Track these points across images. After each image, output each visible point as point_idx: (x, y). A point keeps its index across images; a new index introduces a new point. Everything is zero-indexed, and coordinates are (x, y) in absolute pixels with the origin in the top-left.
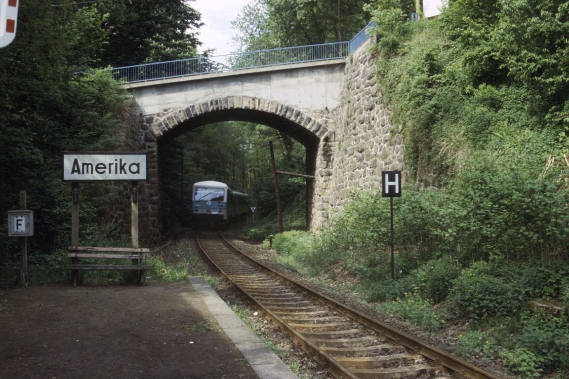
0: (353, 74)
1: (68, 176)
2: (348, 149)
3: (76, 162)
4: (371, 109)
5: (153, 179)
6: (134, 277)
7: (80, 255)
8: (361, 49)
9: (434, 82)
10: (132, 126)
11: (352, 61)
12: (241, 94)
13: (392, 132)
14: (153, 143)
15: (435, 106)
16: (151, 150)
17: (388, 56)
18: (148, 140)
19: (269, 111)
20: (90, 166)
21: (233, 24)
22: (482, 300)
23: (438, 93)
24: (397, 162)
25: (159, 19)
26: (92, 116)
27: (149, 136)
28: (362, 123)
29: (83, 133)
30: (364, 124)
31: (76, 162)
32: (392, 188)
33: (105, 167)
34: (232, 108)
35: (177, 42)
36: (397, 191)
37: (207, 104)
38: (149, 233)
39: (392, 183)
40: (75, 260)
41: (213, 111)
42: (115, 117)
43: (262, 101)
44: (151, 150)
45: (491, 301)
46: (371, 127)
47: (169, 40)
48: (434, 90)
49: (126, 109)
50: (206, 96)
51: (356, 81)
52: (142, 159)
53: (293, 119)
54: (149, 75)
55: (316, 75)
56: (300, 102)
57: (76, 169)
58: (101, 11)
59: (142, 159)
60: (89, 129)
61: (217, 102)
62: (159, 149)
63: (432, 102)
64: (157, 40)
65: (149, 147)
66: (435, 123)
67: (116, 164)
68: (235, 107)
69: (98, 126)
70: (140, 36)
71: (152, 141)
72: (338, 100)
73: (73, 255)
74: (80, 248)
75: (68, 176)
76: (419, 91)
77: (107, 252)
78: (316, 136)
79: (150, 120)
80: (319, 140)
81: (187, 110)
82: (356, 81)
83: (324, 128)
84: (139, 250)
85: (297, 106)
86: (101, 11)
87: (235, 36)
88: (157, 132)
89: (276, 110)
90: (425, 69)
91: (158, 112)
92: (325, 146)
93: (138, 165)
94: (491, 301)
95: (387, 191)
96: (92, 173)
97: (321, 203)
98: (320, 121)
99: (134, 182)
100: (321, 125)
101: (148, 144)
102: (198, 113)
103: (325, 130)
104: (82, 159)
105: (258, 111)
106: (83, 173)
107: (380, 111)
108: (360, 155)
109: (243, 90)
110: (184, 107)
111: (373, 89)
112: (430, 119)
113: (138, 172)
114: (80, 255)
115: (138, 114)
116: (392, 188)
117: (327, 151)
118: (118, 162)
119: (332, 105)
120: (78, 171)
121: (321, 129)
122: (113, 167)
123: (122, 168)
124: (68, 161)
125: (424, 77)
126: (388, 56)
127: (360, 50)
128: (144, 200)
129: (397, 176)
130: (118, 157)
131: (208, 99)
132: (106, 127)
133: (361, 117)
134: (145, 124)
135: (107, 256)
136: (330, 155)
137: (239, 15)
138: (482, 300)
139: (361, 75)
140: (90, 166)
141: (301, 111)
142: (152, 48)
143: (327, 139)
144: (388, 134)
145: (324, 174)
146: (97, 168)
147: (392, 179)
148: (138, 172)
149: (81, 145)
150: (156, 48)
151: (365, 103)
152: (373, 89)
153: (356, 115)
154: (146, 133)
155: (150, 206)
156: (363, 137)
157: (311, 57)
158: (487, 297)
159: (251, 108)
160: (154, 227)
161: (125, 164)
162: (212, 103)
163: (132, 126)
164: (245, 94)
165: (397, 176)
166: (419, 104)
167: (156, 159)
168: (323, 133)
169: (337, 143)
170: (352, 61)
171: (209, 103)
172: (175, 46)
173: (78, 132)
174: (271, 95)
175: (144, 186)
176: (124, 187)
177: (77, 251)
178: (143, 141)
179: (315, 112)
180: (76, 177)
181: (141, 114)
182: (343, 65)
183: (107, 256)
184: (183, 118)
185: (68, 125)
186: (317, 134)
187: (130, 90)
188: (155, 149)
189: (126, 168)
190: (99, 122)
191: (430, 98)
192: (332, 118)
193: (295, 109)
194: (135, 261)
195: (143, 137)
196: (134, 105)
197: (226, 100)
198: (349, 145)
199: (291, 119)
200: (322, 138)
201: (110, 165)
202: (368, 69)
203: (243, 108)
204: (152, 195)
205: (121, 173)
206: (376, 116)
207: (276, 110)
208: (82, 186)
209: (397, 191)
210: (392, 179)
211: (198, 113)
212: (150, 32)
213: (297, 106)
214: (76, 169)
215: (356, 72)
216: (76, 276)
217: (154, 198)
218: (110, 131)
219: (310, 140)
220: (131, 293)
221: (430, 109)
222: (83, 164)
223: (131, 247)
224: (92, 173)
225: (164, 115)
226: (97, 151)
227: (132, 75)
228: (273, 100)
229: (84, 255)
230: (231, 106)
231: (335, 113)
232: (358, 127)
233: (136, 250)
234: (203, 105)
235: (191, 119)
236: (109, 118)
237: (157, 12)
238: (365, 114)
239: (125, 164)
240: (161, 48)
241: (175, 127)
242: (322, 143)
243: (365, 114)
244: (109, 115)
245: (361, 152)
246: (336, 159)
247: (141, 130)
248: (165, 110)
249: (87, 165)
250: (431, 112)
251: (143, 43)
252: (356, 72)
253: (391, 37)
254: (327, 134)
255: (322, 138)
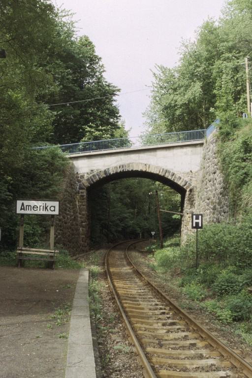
0: (207, 151)
1: (19, 211)
2: (202, 197)
3: (23, 204)
4: (215, 173)
5: (84, 212)
6: (50, 265)
7: (23, 252)
8: (212, 133)
9: (247, 159)
10: (71, 180)
11: (206, 142)
12: (137, 162)
13: (224, 188)
14: (84, 190)
15: (245, 173)
16: (83, 194)
17: (223, 141)
18: (81, 188)
19: (155, 173)
20: (30, 207)
21: (143, 114)
22: (223, 285)
23: (248, 165)
24: (226, 207)
25: (91, 114)
26: (46, 174)
27: (81, 186)
28: (210, 182)
29: (40, 185)
30: (211, 182)
31: (23, 204)
32: (197, 224)
33: (37, 208)
34: (132, 171)
35: (103, 128)
36: (200, 225)
37: (117, 167)
38: (79, 245)
39: (197, 221)
40: (21, 254)
41: (120, 172)
42: (60, 175)
43: (151, 166)
44: (83, 194)
45: (228, 286)
46: (214, 185)
47: (97, 126)
48: (246, 163)
49: (68, 170)
50: (116, 162)
51: (208, 155)
52: (56, 204)
53: (170, 177)
54: (84, 150)
55: (185, 150)
56: (175, 167)
57: (23, 208)
59: (56, 204)
60: (45, 182)
61: (123, 166)
62: (87, 194)
63: (244, 171)
64: (90, 127)
65: (82, 193)
66: (244, 184)
68: (134, 170)
69: (50, 180)
70: (80, 123)
71: (83, 189)
72: (198, 166)
73: (20, 252)
74: (23, 248)
75: (19, 211)
76: (237, 164)
77: (36, 251)
78: (184, 189)
79: (82, 177)
80: (186, 191)
81: (105, 171)
82: (208, 155)
83: (189, 184)
84: (53, 251)
85: (172, 170)
87: (144, 122)
88: (87, 184)
89: (160, 172)
90: (242, 150)
91: (87, 172)
92: (189, 195)
93: (54, 207)
94: (228, 286)
95: (194, 225)
96: (31, 210)
97: (186, 231)
98: (187, 179)
99: (53, 216)
100: (187, 182)
101: (81, 191)
102: (111, 173)
103: (190, 185)
104: (26, 203)
105: (148, 172)
107: (219, 175)
108: (208, 201)
109: (139, 159)
110: (103, 169)
111: (216, 160)
112: (242, 181)
113: (54, 210)
114: (23, 252)
115: (76, 173)
116: (197, 224)
117: (191, 198)
118: (44, 205)
119: (195, 168)
120: (24, 209)
121: (187, 184)
122: (42, 207)
123: (46, 208)
124: (19, 203)
125: (242, 155)
126: (223, 141)
127: (210, 136)
128: (77, 225)
129: (200, 217)
130: (43, 202)
131: (118, 164)
132: (54, 180)
133: (209, 178)
134: (79, 179)
135: (36, 253)
136: (193, 201)
137: (147, 108)
138: (223, 285)
139: (211, 151)
140: (30, 207)
141: (175, 172)
142: (87, 132)
143: (191, 191)
144: (222, 189)
145: (189, 212)
146: (33, 208)
147: (197, 218)
148: (54, 210)
149: (38, 191)
150: (89, 131)
151: (212, 169)
152: (216, 160)
153: (207, 176)
154: (80, 185)
155: (81, 229)
156: (210, 190)
157: (185, 139)
158: (226, 284)
159: (144, 170)
160: (83, 241)
162: (120, 167)
163: (71, 180)
164: (141, 162)
165: (200, 217)
166: (236, 172)
167: (85, 200)
168: (189, 186)
169: (197, 193)
170: (206, 142)
171: (118, 167)
172: (101, 130)
173: (37, 184)
174: (156, 163)
175: (77, 216)
176: (63, 217)
177: (21, 250)
178: (78, 189)
179: (183, 173)
180: (23, 212)
181: (77, 173)
182: (202, 144)
183: (36, 253)
184: (103, 175)
185: (32, 180)
186: (185, 187)
187: (71, 158)
188: (85, 194)
189: (48, 208)
190: (51, 177)
191: (243, 168)
192: (194, 178)
193: (171, 171)
194: (51, 257)
195: (78, 187)
196: (72, 168)
197: (129, 165)
198: (203, 195)
199: (169, 178)
200: (188, 190)
201: (40, 206)
202: (215, 148)
203: (139, 170)
204: (82, 222)
206: (217, 178)
207: (160, 172)
208: (25, 217)
209: (200, 225)
210: (197, 218)
211: (111, 173)
212: (87, 122)
213: (172, 170)
214: (23, 208)
215: (209, 149)
216: (21, 263)
217: (84, 224)
218: (57, 183)
219: (181, 190)
220: (47, 272)
221: (242, 175)
222: (27, 206)
223: (50, 249)
224: (31, 210)
225: (91, 173)
226: (34, 199)
227: (71, 150)
228: (157, 165)
229: (25, 252)
230: (132, 169)
231: (196, 174)
232: (208, 184)
233: (52, 251)
234: (115, 168)
235: (107, 177)
236: (56, 176)
237: (91, 110)
238: (212, 176)
240: (93, 132)
241: (97, 181)
242: (188, 193)
243: (212, 176)
244: (56, 174)
245: (208, 200)
246: (196, 203)
247: (77, 183)
248: (92, 171)
249: (29, 206)
250: (242, 177)
251: (82, 128)
252: (209, 149)
253: (227, 129)
254: (191, 187)
255: (188, 190)
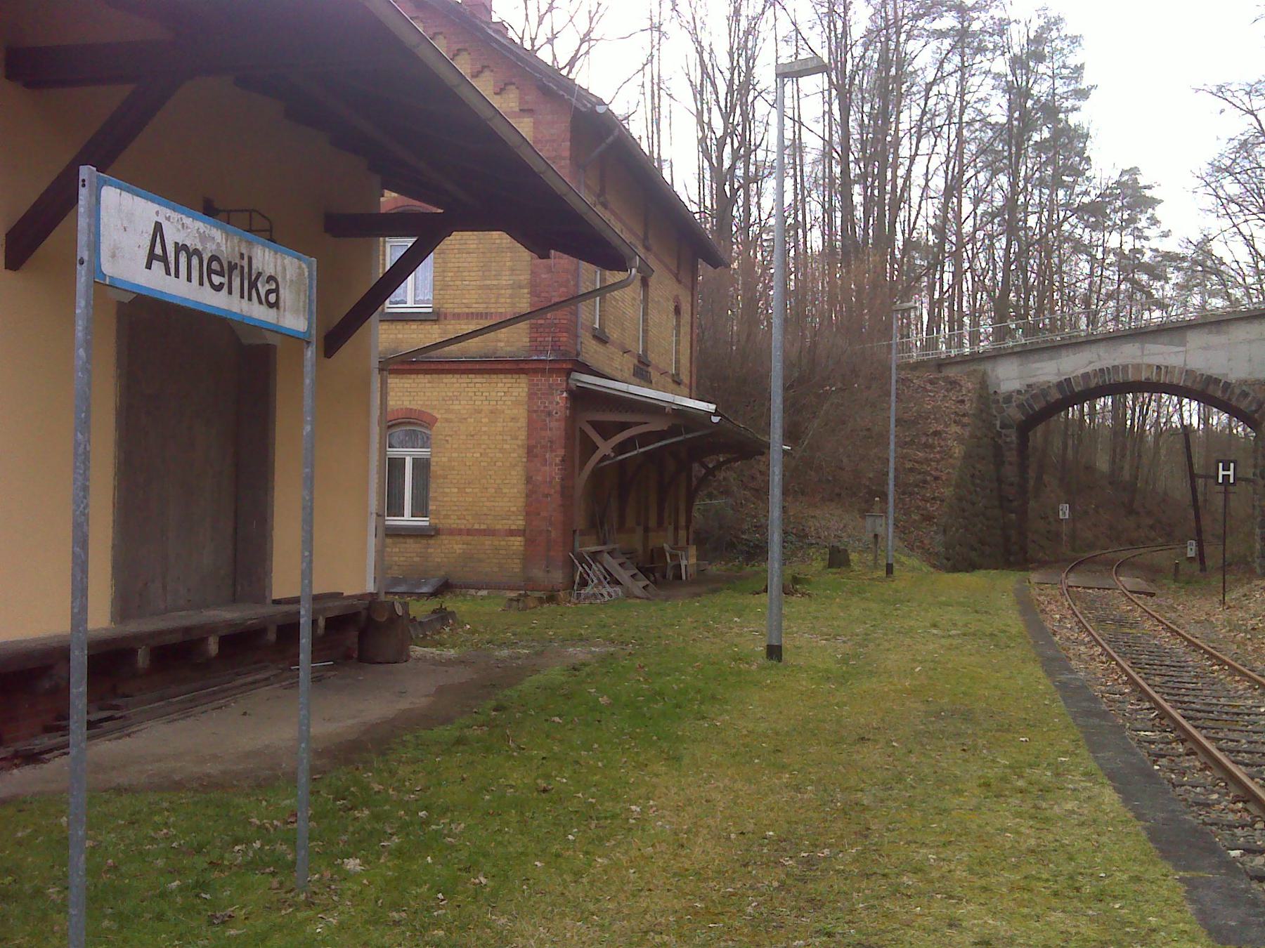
20: (195, 261)
57: (158, 250)
58: (716, 413)
67: (242, 267)
86: (716, 413)
106: (177, 276)
161: (259, 274)
205: (250, 299)
214: (158, 250)
239: (259, 274)
